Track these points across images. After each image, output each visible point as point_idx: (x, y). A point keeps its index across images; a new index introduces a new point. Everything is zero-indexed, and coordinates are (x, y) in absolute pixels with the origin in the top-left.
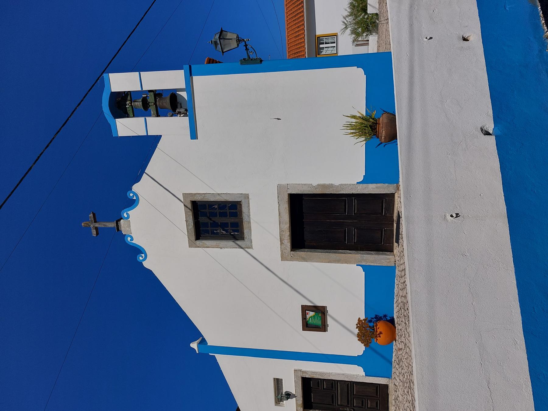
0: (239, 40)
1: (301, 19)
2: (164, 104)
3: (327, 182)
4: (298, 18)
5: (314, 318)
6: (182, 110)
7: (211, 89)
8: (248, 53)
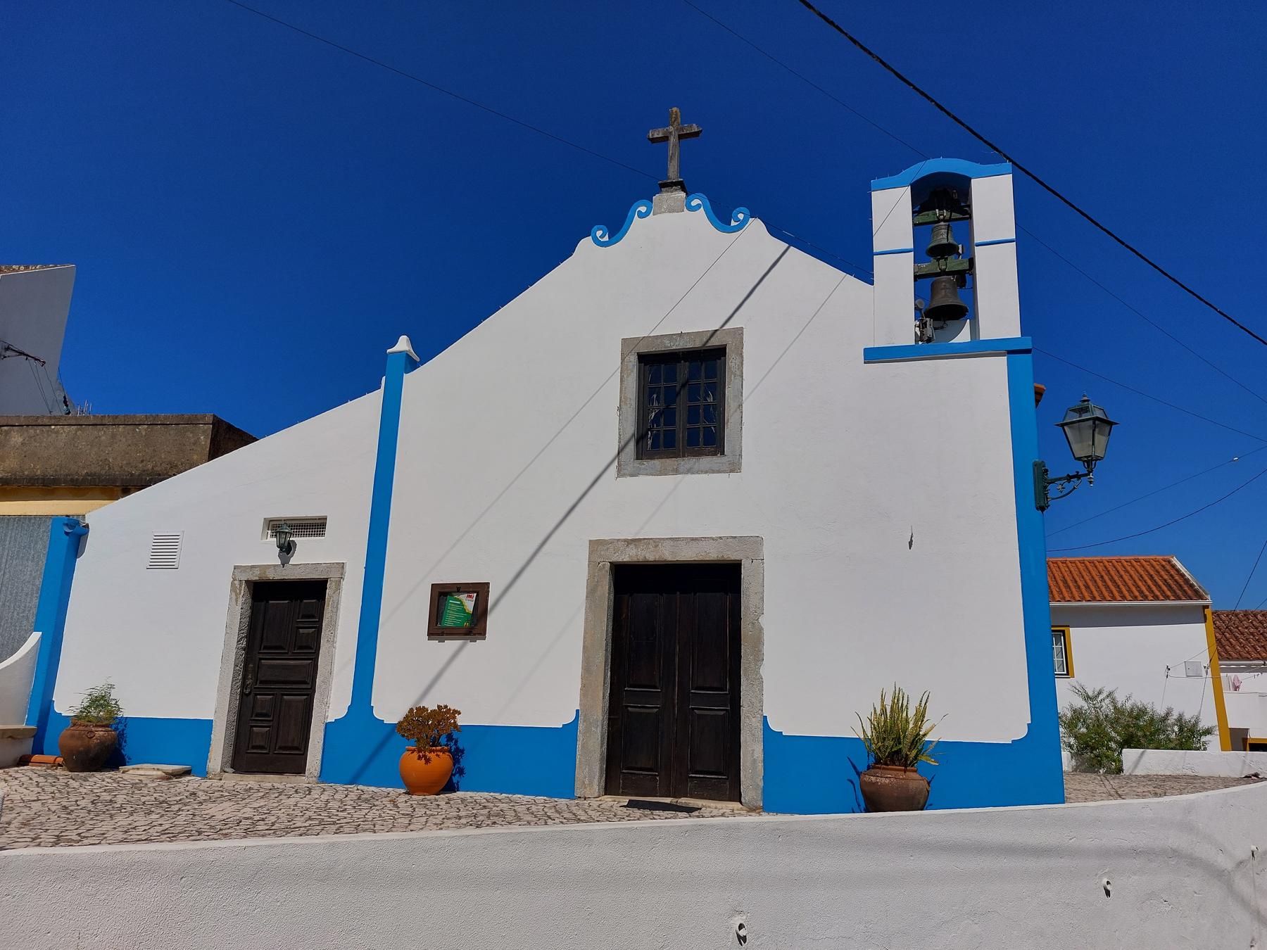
0: (1089, 461)
1: (1106, 594)
2: (943, 292)
3: (767, 649)
4: (1107, 587)
5: (458, 611)
6: (929, 331)
7: (976, 398)
8: (1060, 479)
